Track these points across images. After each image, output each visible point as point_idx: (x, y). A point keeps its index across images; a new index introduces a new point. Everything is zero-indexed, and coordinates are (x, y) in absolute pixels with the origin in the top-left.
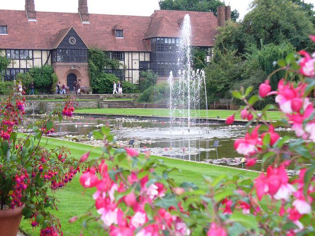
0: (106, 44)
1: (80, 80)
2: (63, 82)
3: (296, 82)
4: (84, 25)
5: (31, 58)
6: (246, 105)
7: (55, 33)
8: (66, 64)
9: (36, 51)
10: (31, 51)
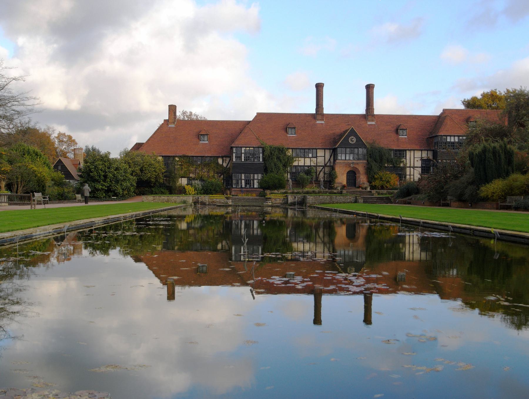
0: (387, 143)
2: (342, 179)
3: (508, 90)
6: (11, 191)
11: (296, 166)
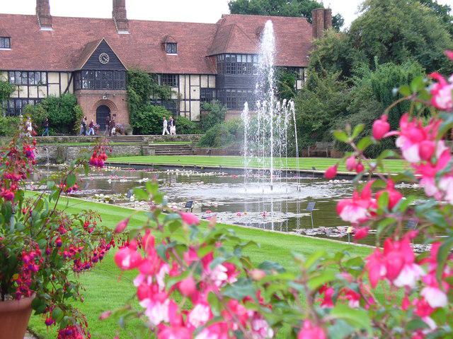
0: (152, 63)
1: (114, 115)
2: (90, 117)
4: (121, 35)
5: (44, 83)
7: (79, 48)
8: (96, 91)
9: (52, 73)
10: (45, 73)
11: (15, 99)
